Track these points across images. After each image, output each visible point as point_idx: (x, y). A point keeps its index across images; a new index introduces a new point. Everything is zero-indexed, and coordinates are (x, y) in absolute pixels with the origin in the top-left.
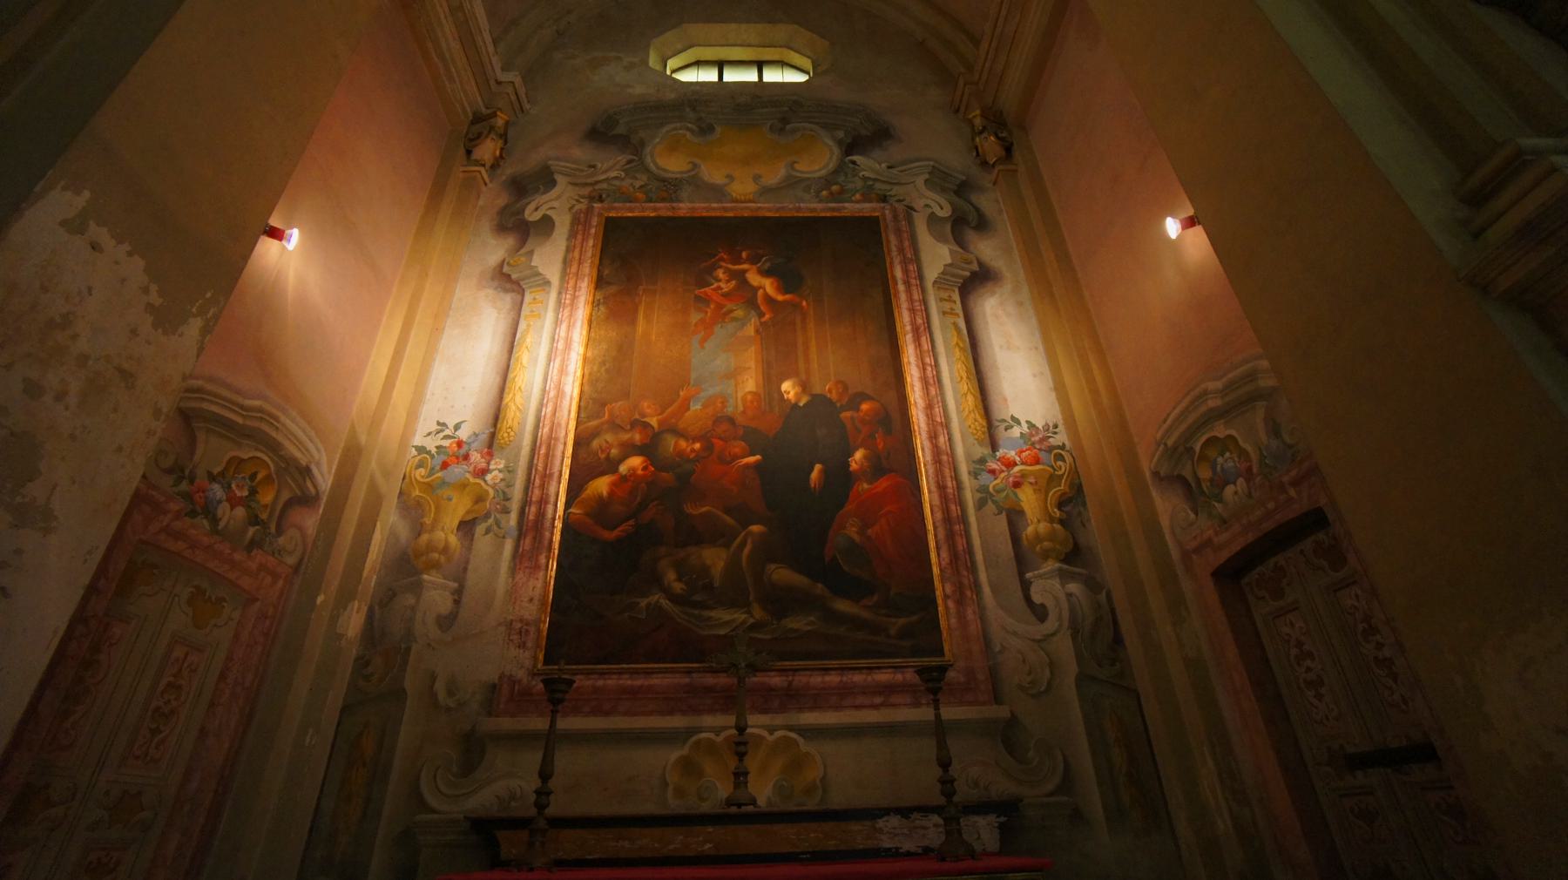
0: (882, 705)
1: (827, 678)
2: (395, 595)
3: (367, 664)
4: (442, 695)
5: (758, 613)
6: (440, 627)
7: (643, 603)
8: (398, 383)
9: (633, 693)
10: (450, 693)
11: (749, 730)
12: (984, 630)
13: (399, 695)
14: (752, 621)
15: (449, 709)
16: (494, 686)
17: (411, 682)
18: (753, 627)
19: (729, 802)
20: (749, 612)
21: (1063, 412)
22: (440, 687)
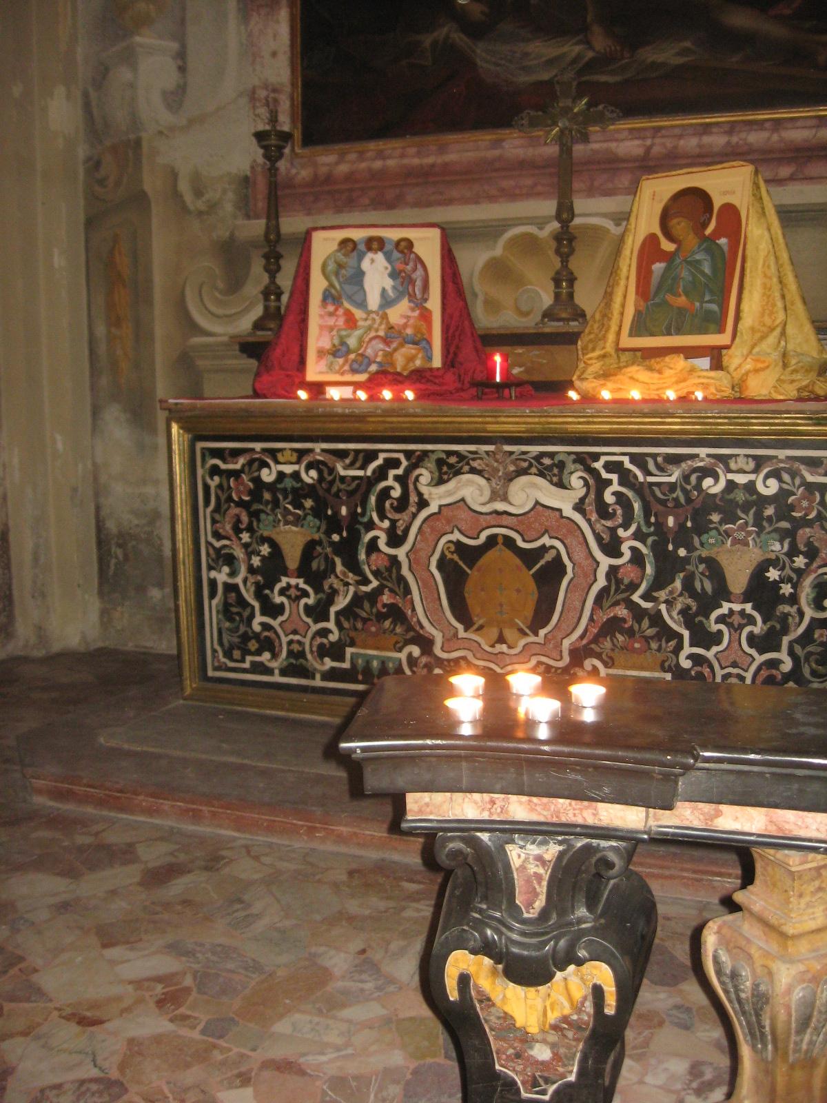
0: (792, 178)
1: (707, 139)
2: (107, 70)
3: (98, 165)
4: (188, 198)
5: (601, 42)
6: (169, 107)
7: (427, 40)
8: (805, 202)
9: (425, 176)
10: (198, 193)
11: (577, 221)
12: (637, 381)
13: (140, 200)
14: (590, 54)
15: (200, 213)
16: (246, 180)
17: (151, 183)
18: (590, 66)
19: (548, 315)
20: (588, 43)
21: (463, 736)
22: (184, 186)
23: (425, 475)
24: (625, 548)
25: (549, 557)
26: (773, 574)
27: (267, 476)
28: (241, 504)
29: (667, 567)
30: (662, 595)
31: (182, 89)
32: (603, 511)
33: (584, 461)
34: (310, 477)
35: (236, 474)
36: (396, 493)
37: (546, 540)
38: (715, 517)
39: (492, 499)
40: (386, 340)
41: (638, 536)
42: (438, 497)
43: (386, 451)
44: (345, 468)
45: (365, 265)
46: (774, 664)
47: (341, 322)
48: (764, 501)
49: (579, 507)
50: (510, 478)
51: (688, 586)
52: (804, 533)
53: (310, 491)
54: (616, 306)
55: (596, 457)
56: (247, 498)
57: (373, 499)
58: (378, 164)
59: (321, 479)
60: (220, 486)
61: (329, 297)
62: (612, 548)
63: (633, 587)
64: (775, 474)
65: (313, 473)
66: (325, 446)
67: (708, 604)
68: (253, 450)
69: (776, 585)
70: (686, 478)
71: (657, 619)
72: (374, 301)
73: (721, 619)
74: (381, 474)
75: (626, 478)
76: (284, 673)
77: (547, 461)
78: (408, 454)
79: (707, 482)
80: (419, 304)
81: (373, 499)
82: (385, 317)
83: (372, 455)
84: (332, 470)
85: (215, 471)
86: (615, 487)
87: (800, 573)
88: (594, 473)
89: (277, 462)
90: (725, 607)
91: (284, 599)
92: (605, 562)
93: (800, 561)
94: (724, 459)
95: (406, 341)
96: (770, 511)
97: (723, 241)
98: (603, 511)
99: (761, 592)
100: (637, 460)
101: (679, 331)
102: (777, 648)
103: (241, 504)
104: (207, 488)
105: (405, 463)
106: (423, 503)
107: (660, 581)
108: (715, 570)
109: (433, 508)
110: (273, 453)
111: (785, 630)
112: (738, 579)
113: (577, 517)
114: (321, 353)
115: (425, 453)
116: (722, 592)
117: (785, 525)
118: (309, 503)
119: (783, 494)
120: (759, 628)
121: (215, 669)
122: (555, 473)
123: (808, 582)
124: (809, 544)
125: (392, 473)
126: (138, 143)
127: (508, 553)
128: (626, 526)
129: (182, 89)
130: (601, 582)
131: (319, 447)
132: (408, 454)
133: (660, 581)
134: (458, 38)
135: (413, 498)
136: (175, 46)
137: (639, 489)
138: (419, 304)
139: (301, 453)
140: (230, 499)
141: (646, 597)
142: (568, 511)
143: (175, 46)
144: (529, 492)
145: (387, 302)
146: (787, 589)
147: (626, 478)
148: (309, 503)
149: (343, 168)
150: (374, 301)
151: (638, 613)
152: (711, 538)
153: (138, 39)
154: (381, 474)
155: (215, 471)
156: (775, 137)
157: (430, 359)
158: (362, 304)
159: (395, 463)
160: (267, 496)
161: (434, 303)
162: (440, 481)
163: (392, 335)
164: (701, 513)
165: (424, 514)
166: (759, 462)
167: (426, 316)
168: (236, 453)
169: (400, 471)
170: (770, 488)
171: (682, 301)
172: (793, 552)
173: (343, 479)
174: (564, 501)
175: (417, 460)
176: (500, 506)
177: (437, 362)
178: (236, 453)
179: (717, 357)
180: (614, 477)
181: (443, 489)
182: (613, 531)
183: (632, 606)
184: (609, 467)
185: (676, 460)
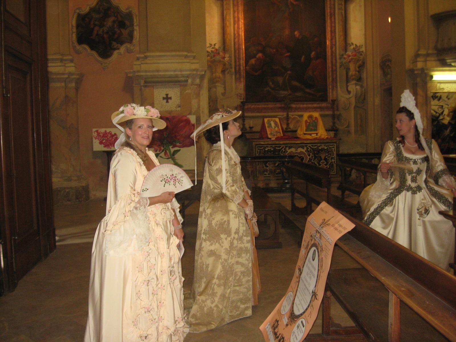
2: (211, 88)
5: (290, 92)
7: (265, 89)
14: (288, 94)
23: (287, 148)
24: (311, 155)
25: (302, 157)
26: (327, 157)
27: (266, 149)
28: (263, 153)
29: (315, 157)
30: (315, 160)
31: (225, 93)
32: (308, 151)
33: (306, 146)
34: (272, 149)
35: (262, 149)
36: (284, 151)
37: (302, 155)
38: (320, 151)
39: (296, 151)
40: (276, 132)
41: (312, 154)
42: (289, 151)
43: (282, 146)
44: (277, 148)
45: (271, 123)
46: (327, 167)
47: (270, 130)
48: (325, 149)
49: (306, 151)
50: (297, 148)
51: (318, 160)
52: (330, 152)
53: (272, 151)
54: (303, 128)
55: (307, 145)
56: (263, 152)
57: (281, 152)
58: (258, 106)
59: (274, 150)
60: (259, 151)
61: (268, 127)
62: (309, 155)
63: (312, 160)
64: (326, 146)
65: (273, 149)
66: (275, 145)
67: (320, 161)
68: (264, 146)
69: (327, 158)
70: (317, 147)
71: (314, 163)
72: (273, 128)
73: (321, 163)
74: (282, 148)
75: (311, 148)
76: (268, 175)
77: (302, 146)
78: (285, 146)
79: (319, 148)
80: (278, 127)
81: (281, 152)
82: (275, 130)
83: (281, 146)
84: (275, 148)
85: (259, 149)
86: (310, 149)
87: (329, 157)
88: (307, 147)
89: (268, 148)
90: (322, 161)
91: (268, 165)
92: (309, 157)
93: (329, 156)
94: (321, 145)
95: (278, 132)
96: (326, 150)
97: (316, 121)
98: (308, 151)
99: (325, 159)
100: (312, 146)
101: (312, 131)
102: (327, 165)
103: (263, 153)
104: (257, 152)
105: (285, 147)
106: (287, 152)
107: (315, 159)
108: (320, 157)
109: (288, 152)
110: (267, 147)
111: (328, 163)
112: (323, 157)
113: (305, 152)
114: (269, 134)
115: (287, 146)
116: (321, 159)
117: (327, 152)
118: (272, 153)
119: (327, 148)
120: (325, 163)
121: (334, 145)
122: (303, 147)
123: (330, 158)
124: (330, 154)
125: (283, 148)
126: (217, 101)
127: (298, 157)
128: (311, 153)
129: (225, 93)
130: (308, 159)
131: (274, 146)
132: (285, 146)
133: (315, 159)
134: (270, 90)
135: (286, 151)
136: (223, 86)
137: (313, 149)
138: (278, 127)
139: (271, 147)
140: (261, 153)
141: (313, 161)
142: (304, 152)
143: (223, 86)
144: (300, 150)
145: (275, 128)
146: (328, 159)
147: (311, 148)
148: (272, 153)
149: (253, 107)
150: (273, 128)
151: (312, 163)
152: (320, 154)
153: (217, 84)
154: (282, 148)
155: (259, 149)
156: (312, 106)
157: (281, 135)
158: (272, 128)
159: (284, 147)
160: (266, 152)
161: (280, 128)
162: (289, 149)
163: (276, 132)
164: (319, 151)
165: (287, 153)
166: (325, 145)
167: (279, 129)
168: (262, 147)
169: (284, 148)
170: (326, 148)
171: (312, 128)
172: (329, 155)
173: (277, 149)
174: (304, 151)
175: (286, 147)
176: (296, 152)
177: (282, 135)
178: (262, 147)
179: (317, 134)
180: (309, 148)
181: (289, 150)
182: (309, 154)
183: (312, 162)
184: (309, 146)
185: (316, 145)
